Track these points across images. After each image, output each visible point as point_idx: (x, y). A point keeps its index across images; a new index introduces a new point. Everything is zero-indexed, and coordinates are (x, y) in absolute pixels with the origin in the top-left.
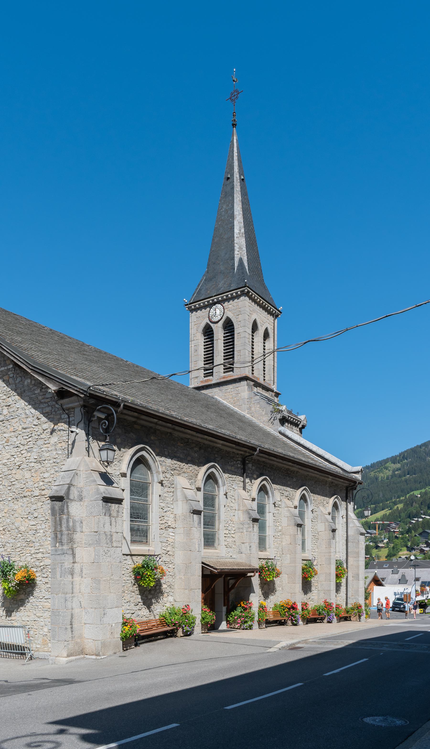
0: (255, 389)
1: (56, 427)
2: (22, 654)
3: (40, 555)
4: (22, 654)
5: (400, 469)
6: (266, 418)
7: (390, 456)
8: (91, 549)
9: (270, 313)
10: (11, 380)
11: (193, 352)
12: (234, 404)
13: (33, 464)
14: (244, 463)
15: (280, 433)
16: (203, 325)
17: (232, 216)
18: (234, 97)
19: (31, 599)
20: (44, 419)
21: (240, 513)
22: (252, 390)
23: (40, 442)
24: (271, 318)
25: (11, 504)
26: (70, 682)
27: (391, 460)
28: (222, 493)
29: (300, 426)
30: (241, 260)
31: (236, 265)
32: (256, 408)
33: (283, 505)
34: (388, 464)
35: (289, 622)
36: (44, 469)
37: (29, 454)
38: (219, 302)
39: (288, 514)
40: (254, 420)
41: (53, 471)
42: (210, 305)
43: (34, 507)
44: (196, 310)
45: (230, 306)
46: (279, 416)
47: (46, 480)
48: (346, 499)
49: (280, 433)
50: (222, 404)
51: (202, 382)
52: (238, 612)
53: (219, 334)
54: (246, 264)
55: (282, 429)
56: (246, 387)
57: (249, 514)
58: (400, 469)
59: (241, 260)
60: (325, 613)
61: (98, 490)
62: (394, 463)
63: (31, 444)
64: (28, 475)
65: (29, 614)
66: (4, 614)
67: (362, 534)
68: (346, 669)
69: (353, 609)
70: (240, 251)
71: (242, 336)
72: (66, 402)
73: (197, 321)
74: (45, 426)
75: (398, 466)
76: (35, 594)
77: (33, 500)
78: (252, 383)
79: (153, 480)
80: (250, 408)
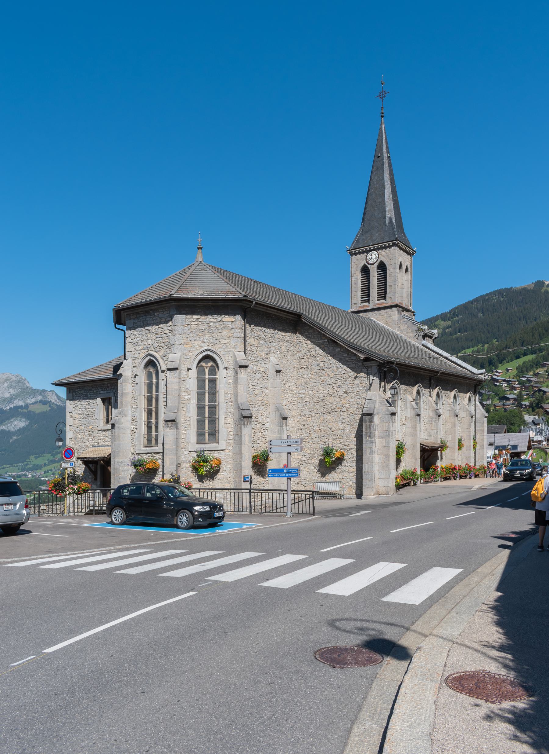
0: (403, 313)
1: (358, 375)
2: (334, 497)
3: (347, 443)
4: (334, 497)
5: (450, 327)
6: (412, 335)
7: (439, 313)
8: (383, 440)
9: (409, 254)
10: (325, 348)
11: (353, 285)
12: (387, 324)
13: (342, 394)
14: (430, 381)
15: (423, 345)
16: (361, 265)
17: (383, 186)
18: (382, 95)
19: (340, 467)
20: (349, 370)
21: (430, 412)
22: (401, 314)
23: (347, 383)
24: (409, 257)
25: (326, 415)
26: (404, 503)
27: (441, 318)
28: (422, 401)
29: (434, 338)
30: (390, 219)
31: (387, 222)
32: (404, 327)
33: (446, 403)
34: (438, 322)
35: (452, 478)
36: (350, 397)
37: (339, 389)
38: (374, 250)
39: (450, 409)
40: (403, 336)
41: (356, 398)
42: (367, 252)
43: (343, 417)
44: (356, 254)
45: (384, 253)
46: (422, 334)
47: (351, 403)
48: (475, 393)
49: (423, 345)
50: (377, 324)
51: (360, 307)
52: (431, 471)
53: (374, 273)
54: (394, 221)
55: (424, 342)
56: (396, 312)
57: (436, 412)
58: (450, 327)
59: (390, 219)
60: (468, 472)
61: (388, 409)
62: (444, 321)
63: (340, 384)
64: (338, 400)
65: (338, 475)
66: (320, 475)
67: (486, 417)
68: (85, 638)
69: (480, 469)
70: (390, 213)
71: (393, 275)
72: (367, 364)
73: (358, 261)
74: (351, 374)
75: (449, 323)
76: (343, 464)
77: (341, 413)
78: (401, 309)
79: (398, 398)
80: (399, 327)
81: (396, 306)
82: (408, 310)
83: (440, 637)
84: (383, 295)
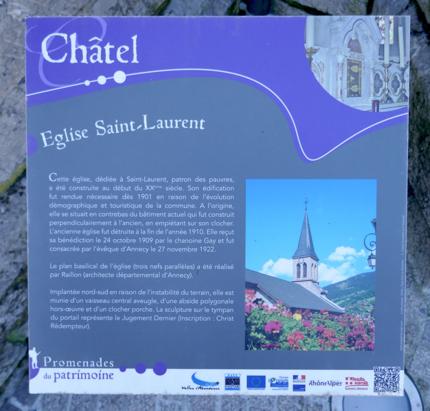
17: (306, 235)
18: (306, 202)
53: (302, 266)
55: (321, 296)
70: (308, 244)
81: (310, 280)
82: (316, 282)
83: (309, 280)
84: (305, 276)
